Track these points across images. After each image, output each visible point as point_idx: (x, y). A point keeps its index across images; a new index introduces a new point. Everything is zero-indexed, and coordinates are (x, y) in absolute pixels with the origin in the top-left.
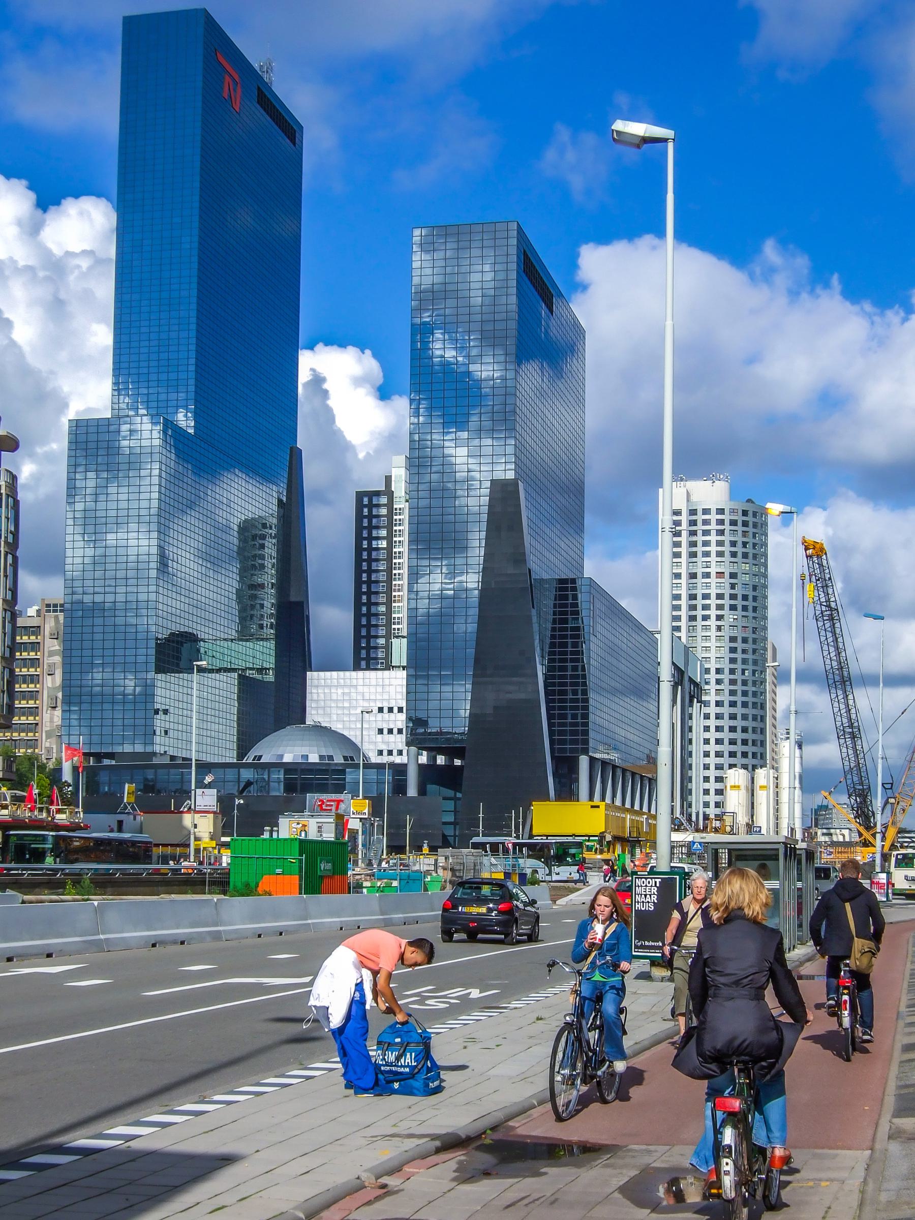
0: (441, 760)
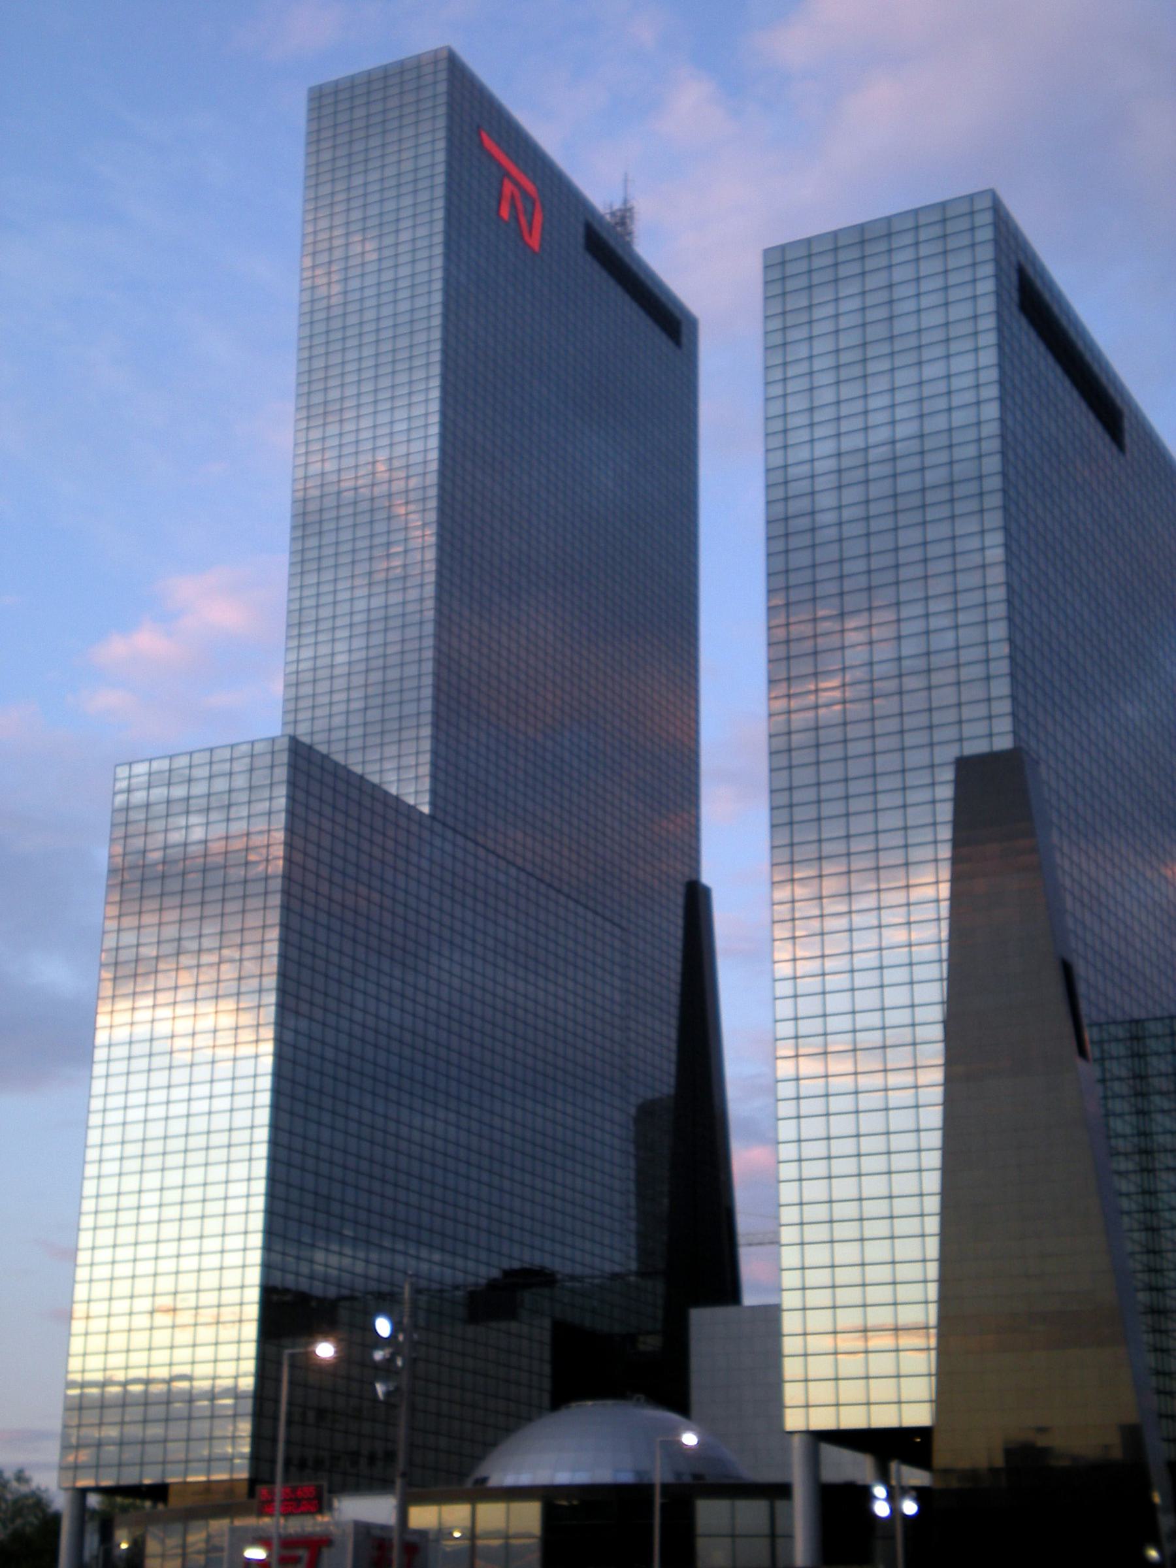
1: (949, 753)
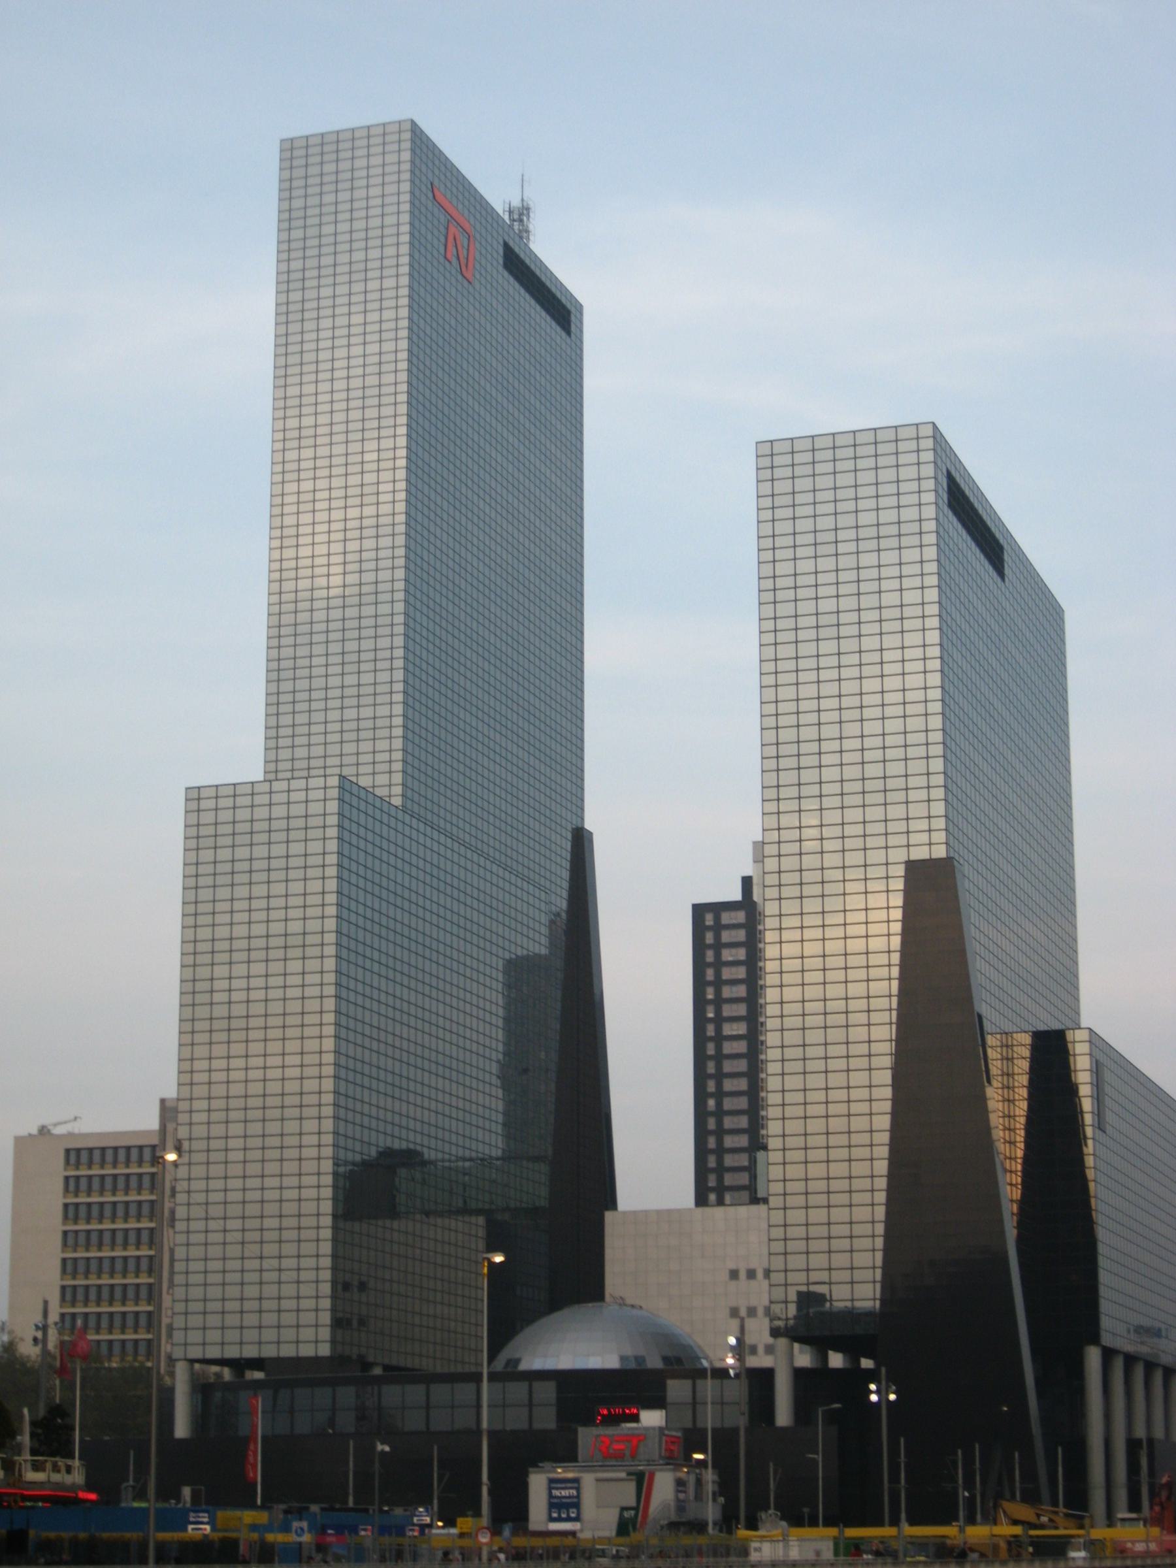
0: (836, 1360)
1: (900, 855)
